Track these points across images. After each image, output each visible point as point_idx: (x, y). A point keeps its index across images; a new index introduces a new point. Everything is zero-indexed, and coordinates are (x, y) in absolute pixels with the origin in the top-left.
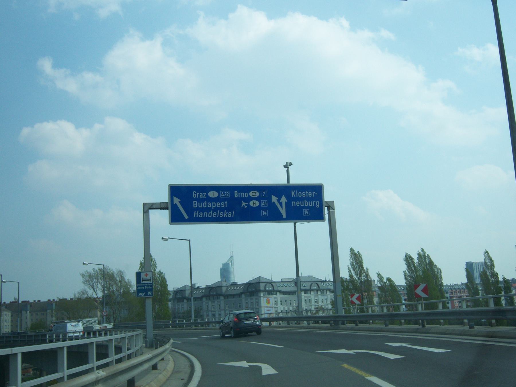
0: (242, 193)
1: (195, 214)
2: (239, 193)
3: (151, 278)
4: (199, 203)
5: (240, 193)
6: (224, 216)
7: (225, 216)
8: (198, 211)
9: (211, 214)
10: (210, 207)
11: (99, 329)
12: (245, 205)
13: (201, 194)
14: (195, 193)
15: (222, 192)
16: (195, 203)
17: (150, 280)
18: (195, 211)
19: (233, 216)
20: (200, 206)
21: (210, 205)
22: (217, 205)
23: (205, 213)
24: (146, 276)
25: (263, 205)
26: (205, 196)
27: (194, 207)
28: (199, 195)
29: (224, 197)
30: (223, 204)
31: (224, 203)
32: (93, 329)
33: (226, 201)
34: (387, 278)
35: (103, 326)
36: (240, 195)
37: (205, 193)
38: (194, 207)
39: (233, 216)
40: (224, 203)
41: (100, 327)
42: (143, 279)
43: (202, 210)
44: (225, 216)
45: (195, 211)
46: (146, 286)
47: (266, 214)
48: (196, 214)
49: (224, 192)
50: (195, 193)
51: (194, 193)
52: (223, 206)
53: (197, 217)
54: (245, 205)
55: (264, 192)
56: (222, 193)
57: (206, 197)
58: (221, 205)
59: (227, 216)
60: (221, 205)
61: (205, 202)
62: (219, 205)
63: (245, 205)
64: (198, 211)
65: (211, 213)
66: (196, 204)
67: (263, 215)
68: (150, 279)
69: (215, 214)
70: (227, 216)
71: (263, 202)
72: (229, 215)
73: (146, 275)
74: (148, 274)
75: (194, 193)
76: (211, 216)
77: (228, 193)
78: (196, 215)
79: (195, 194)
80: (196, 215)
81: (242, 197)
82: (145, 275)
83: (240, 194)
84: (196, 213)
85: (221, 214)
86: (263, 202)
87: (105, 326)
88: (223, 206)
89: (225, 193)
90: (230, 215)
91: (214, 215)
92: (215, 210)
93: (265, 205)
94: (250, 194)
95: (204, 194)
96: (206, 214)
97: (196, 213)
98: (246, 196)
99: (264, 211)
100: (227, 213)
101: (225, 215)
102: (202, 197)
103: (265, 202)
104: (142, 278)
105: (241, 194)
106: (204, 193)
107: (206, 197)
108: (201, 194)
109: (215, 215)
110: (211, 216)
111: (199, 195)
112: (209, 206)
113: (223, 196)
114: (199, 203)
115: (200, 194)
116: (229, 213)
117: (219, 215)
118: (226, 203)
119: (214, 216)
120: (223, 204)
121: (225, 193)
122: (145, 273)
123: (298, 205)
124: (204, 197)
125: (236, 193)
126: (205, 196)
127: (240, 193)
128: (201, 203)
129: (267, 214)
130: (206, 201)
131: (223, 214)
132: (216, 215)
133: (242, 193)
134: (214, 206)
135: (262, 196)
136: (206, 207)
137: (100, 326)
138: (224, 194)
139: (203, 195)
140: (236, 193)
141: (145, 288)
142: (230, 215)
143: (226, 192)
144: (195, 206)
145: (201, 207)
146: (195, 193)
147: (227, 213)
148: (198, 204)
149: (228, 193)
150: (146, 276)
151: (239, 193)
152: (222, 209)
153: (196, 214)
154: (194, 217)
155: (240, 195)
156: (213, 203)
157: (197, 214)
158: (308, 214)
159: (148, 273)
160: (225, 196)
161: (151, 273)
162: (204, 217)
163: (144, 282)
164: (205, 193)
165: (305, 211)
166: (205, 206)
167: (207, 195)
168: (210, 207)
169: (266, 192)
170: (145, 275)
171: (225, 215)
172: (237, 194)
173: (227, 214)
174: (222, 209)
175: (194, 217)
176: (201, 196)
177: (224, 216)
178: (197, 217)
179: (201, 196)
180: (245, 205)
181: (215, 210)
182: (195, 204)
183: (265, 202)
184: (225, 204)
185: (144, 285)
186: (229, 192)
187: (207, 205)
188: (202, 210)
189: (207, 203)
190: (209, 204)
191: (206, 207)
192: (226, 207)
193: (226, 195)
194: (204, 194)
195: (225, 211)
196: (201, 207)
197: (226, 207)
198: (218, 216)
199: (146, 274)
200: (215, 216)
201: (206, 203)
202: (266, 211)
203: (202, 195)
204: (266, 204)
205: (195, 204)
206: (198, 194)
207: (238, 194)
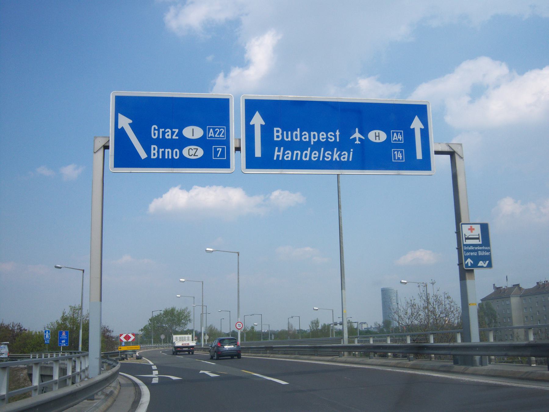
0: (167, 150)
1: (276, 153)
2: (161, 150)
3: (479, 235)
4: (285, 132)
5: (163, 150)
6: (334, 160)
7: (336, 159)
8: (282, 148)
9: (307, 155)
10: (307, 140)
11: (181, 345)
12: (357, 139)
13: (168, 132)
14: (157, 128)
15: (211, 128)
16: (278, 131)
17: (478, 239)
18: (277, 148)
19: (350, 160)
20: (287, 137)
21: (307, 136)
22: (321, 137)
23: (295, 152)
24: (472, 232)
25: (395, 140)
26: (176, 136)
27: (275, 139)
28: (164, 133)
29: (215, 137)
30: (331, 135)
31: (333, 134)
32: (175, 345)
33: (338, 131)
34: (311, 321)
35: (185, 343)
36: (163, 153)
37: (177, 131)
38: (275, 139)
39: (350, 160)
40: (333, 134)
41: (182, 344)
42: (466, 237)
43: (291, 146)
44: (336, 159)
45: (277, 148)
46: (480, 250)
47: (401, 157)
48: (278, 153)
49: (214, 129)
50: (157, 128)
51: (155, 128)
52: (331, 139)
53: (280, 159)
54: (359, 138)
55: (221, 149)
56: (211, 130)
57: (177, 138)
58: (327, 137)
59: (338, 160)
60: (327, 137)
61: (297, 131)
62: (325, 136)
63: (357, 139)
64: (282, 148)
65: (308, 152)
66: (280, 134)
67: (395, 159)
68: (478, 237)
69: (315, 154)
70: (338, 160)
71: (395, 134)
72: (344, 158)
73: (471, 229)
74: (473, 228)
75: (155, 128)
76: (308, 159)
77: (222, 131)
78: (278, 156)
79: (156, 132)
80: (278, 156)
81: (166, 157)
82: (469, 229)
83: (162, 151)
84: (279, 151)
85: (328, 154)
86: (395, 134)
87: (188, 343)
88: (331, 139)
89: (217, 131)
90: (346, 156)
91: (313, 156)
92: (317, 146)
93: (399, 139)
94: (185, 152)
95: (175, 132)
96: (297, 154)
97: (279, 151)
98: (176, 156)
99: (398, 151)
100: (339, 153)
101: (336, 156)
102: (170, 137)
103: (399, 134)
104: (465, 235)
105: (165, 150)
106: (174, 130)
107: (177, 138)
108: (168, 132)
109: (315, 156)
110: (308, 159)
111: (164, 133)
112: (305, 138)
113: (211, 137)
114: (285, 132)
115: (166, 131)
116: (342, 154)
117: (324, 156)
118: (338, 133)
119: (315, 158)
120: (331, 135)
121: (217, 131)
122: (469, 226)
123: (323, 139)
124: (174, 137)
125: (154, 149)
126: (176, 136)
127: (163, 150)
128: (289, 133)
129: (402, 158)
130: (298, 129)
131: (332, 155)
132: (317, 155)
133: (167, 150)
134: (314, 138)
135: (216, 156)
136: (298, 139)
137: (182, 343)
138: (215, 133)
139: (173, 133)
140: (154, 149)
141: (478, 254)
142: (346, 156)
143: (220, 129)
144: (277, 138)
145: (289, 139)
146: (155, 129)
147: (339, 153)
148: (282, 134)
149: (222, 131)
150: (472, 232)
151: (161, 150)
152: (329, 146)
153: (278, 153)
154: (275, 158)
155: (163, 153)
156: (312, 133)
157: (281, 154)
158: (402, 159)
159: (473, 226)
160: (216, 136)
161: (463, 225)
162: (294, 159)
163: (469, 242)
164: (177, 131)
165: (396, 152)
166: (296, 138)
167: (180, 134)
168: (307, 140)
169: (223, 149)
170: (469, 229)
171: (336, 156)
172: (156, 152)
173: (340, 156)
174: (329, 146)
175: (275, 158)
176: (168, 136)
177: (334, 160)
178: (280, 159)
179: (168, 136)
180: (359, 138)
181: (317, 146)
182: (278, 134)
183: (399, 134)
184: (335, 136)
185: (476, 248)
186: (224, 128)
187: (301, 136)
188: (291, 146)
189: (301, 133)
190: (305, 134)
191: (298, 139)
192: (338, 140)
193: (219, 134)
194: (175, 132)
195: (336, 149)
196: (289, 139)
197: (338, 140)
198: (321, 159)
199: (471, 227)
200: (316, 159)
201: (298, 133)
202: (401, 152)
203: (170, 133)
204: (401, 138)
205: (278, 134)
206: (161, 130)
207: (158, 152)
